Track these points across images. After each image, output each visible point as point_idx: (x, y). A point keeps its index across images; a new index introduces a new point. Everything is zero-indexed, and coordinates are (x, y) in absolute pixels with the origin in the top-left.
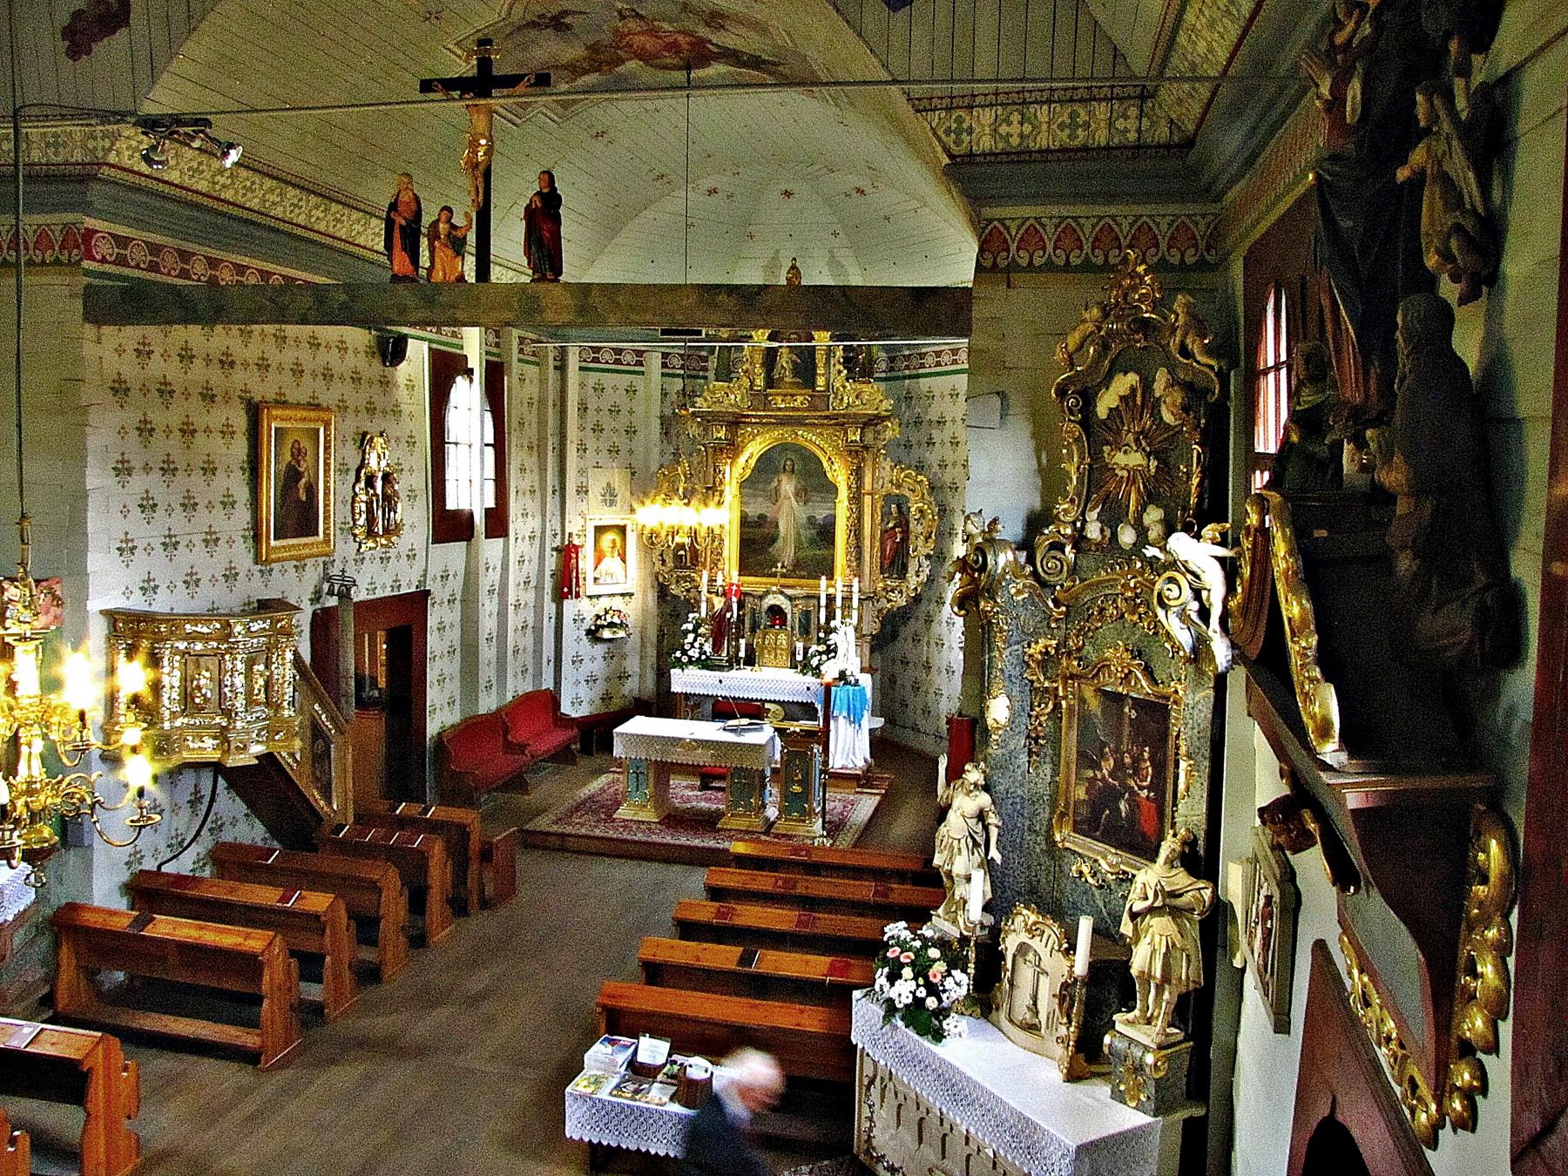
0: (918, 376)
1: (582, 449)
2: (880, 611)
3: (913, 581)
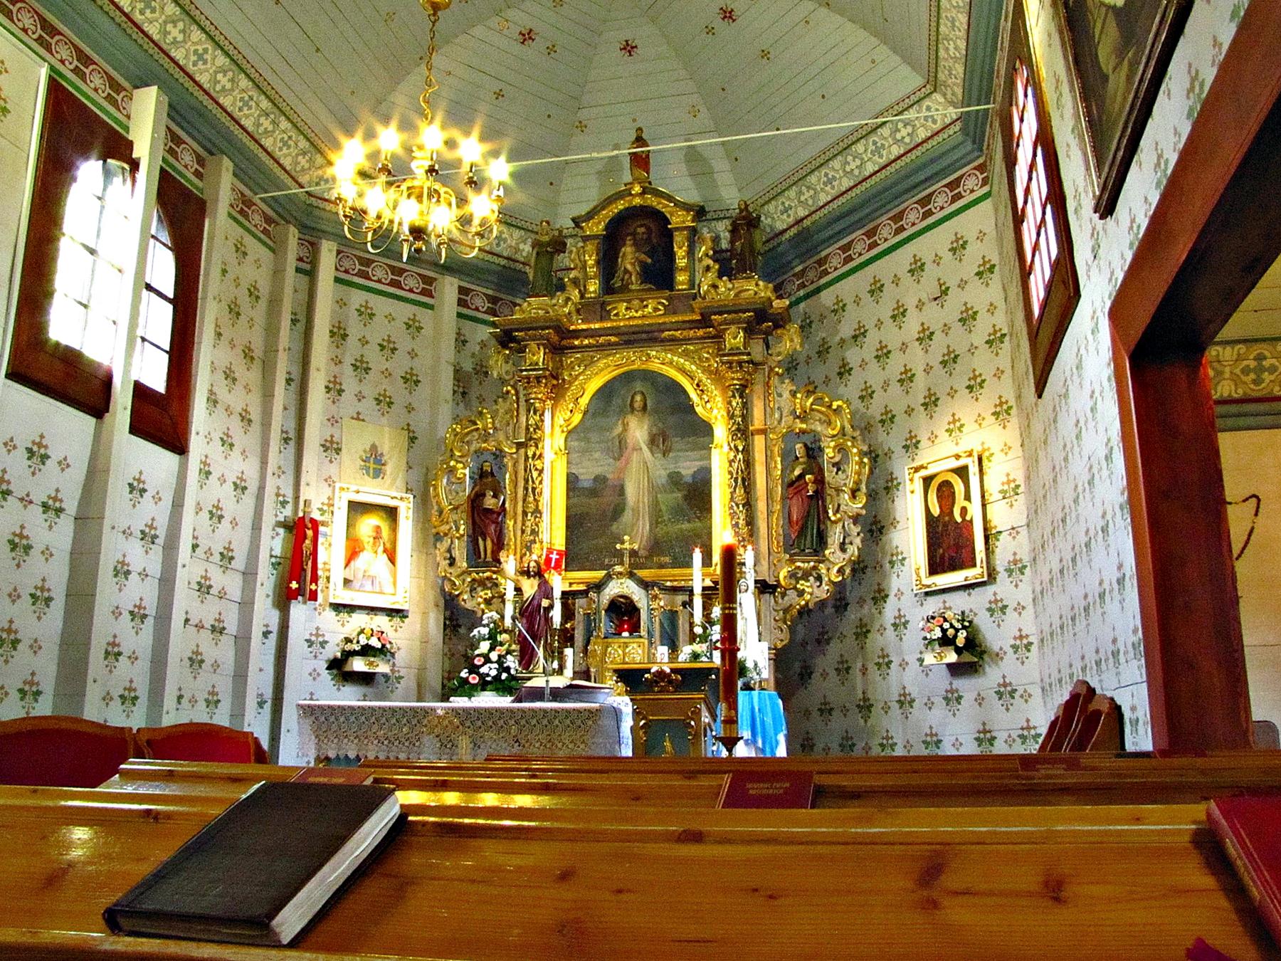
0: (818, 290)
1: (335, 389)
2: (786, 611)
3: (836, 560)
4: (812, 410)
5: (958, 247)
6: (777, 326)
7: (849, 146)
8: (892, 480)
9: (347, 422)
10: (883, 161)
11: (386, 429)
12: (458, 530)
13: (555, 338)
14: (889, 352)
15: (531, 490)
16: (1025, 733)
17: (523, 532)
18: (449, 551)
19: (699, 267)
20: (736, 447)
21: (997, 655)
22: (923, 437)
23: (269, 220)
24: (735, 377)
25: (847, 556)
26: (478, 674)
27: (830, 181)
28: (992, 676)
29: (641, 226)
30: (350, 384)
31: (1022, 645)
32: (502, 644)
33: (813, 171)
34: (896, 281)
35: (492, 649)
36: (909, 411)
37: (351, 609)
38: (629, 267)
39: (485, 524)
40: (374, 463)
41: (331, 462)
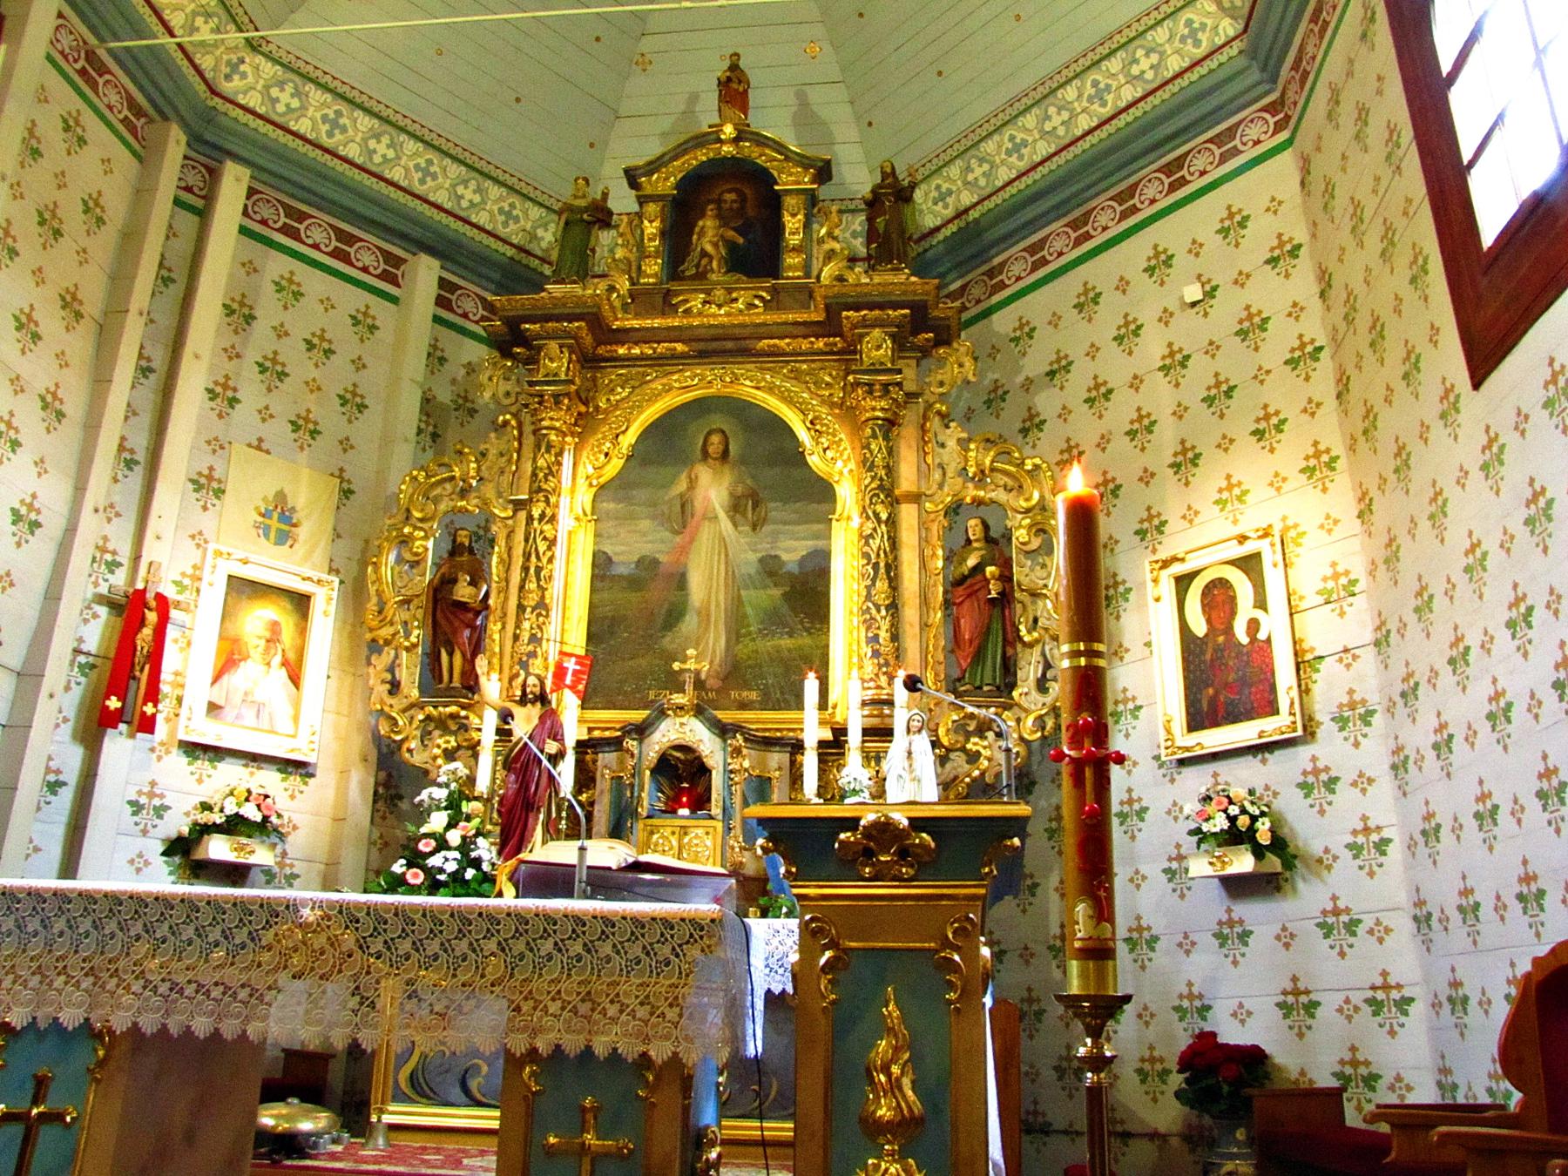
0: (987, 313)
1: (223, 395)
4: (993, 470)
5: (1234, 225)
6: (938, 343)
7: (1053, 91)
8: (1116, 584)
9: (239, 451)
10: (1107, 111)
11: (306, 471)
12: (407, 637)
13: (588, 340)
14: (1110, 391)
15: (534, 569)
16: (1380, 995)
17: (516, 638)
18: (391, 669)
19: (818, 253)
20: (876, 515)
21: (1320, 861)
22: (1172, 514)
23: (139, 112)
24: (876, 407)
25: (1048, 699)
26: (424, 868)
27: (1017, 148)
28: (1307, 899)
29: (729, 191)
30: (251, 392)
31: (1369, 844)
32: (468, 818)
33: (990, 135)
34: (1123, 285)
35: (452, 825)
36: (1147, 477)
37: (216, 753)
38: (709, 248)
39: (453, 621)
40: (280, 521)
41: (205, 508)
